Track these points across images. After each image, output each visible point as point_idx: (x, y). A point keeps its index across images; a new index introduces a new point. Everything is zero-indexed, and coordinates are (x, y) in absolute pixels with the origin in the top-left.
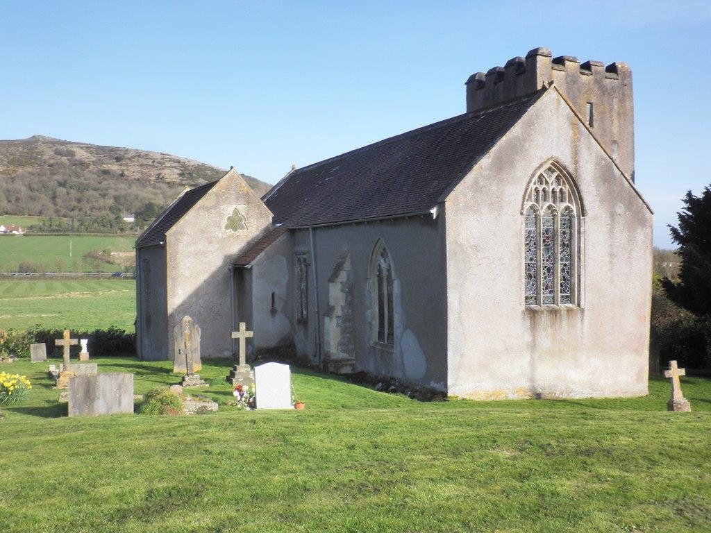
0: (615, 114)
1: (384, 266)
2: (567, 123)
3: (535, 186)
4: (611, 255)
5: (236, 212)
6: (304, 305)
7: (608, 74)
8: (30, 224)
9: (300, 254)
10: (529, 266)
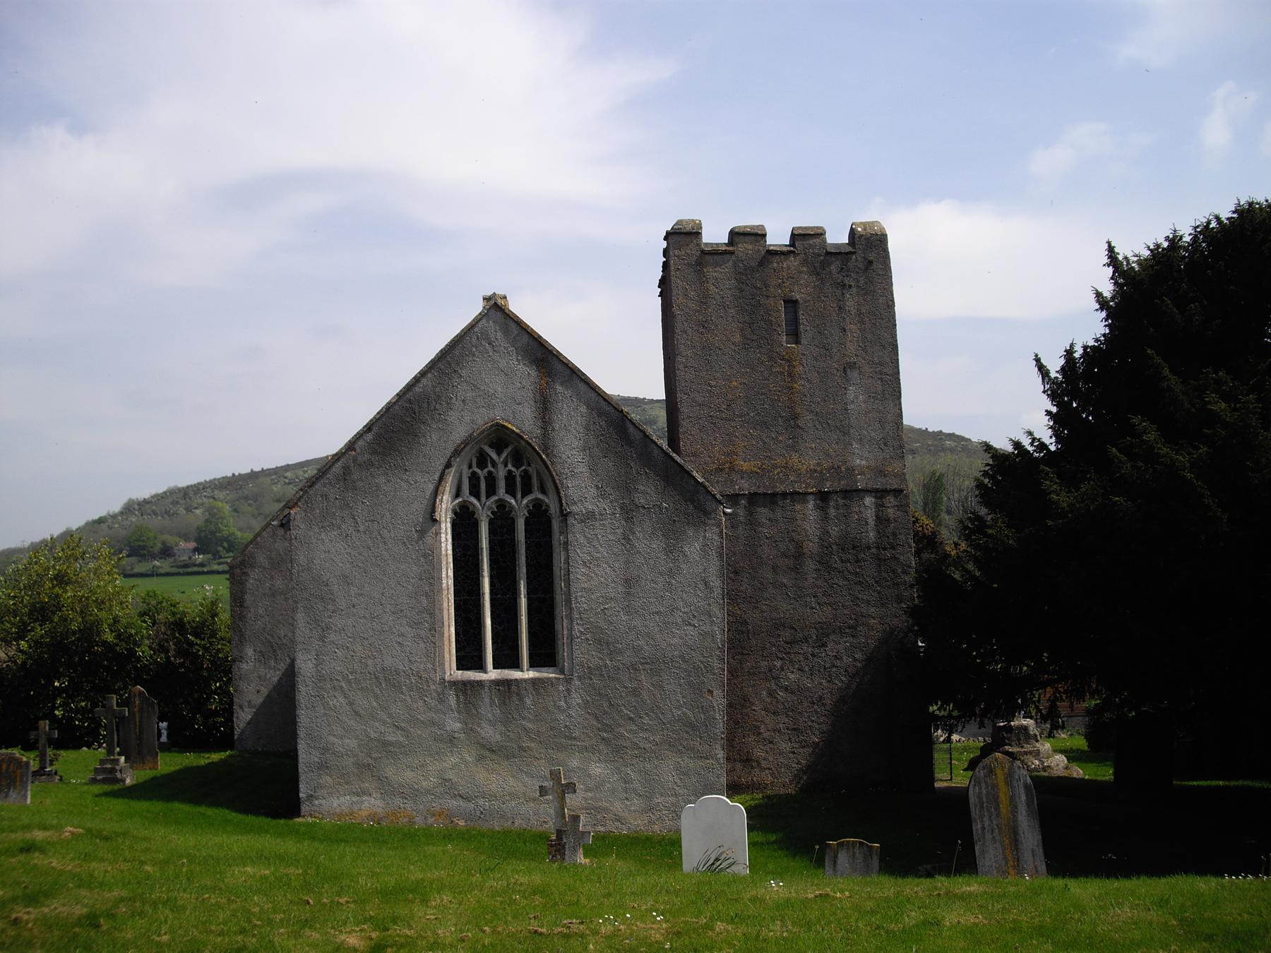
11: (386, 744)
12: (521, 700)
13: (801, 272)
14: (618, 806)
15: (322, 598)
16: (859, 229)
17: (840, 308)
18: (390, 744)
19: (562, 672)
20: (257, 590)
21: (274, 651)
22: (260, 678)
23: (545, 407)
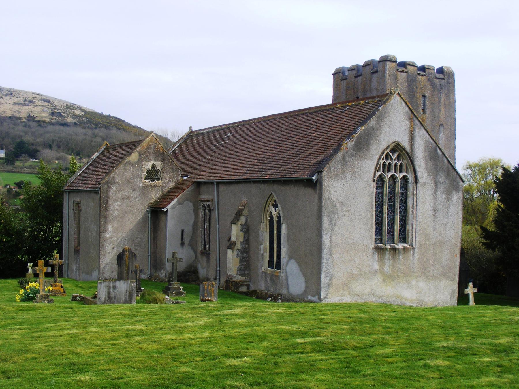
0: (442, 105)
1: (274, 213)
2: (406, 118)
3: (383, 161)
4: (434, 210)
5: (153, 166)
6: (207, 240)
7: (438, 75)
8: (17, 181)
9: (205, 201)
10: (378, 216)
16: (446, 70)
17: (439, 101)
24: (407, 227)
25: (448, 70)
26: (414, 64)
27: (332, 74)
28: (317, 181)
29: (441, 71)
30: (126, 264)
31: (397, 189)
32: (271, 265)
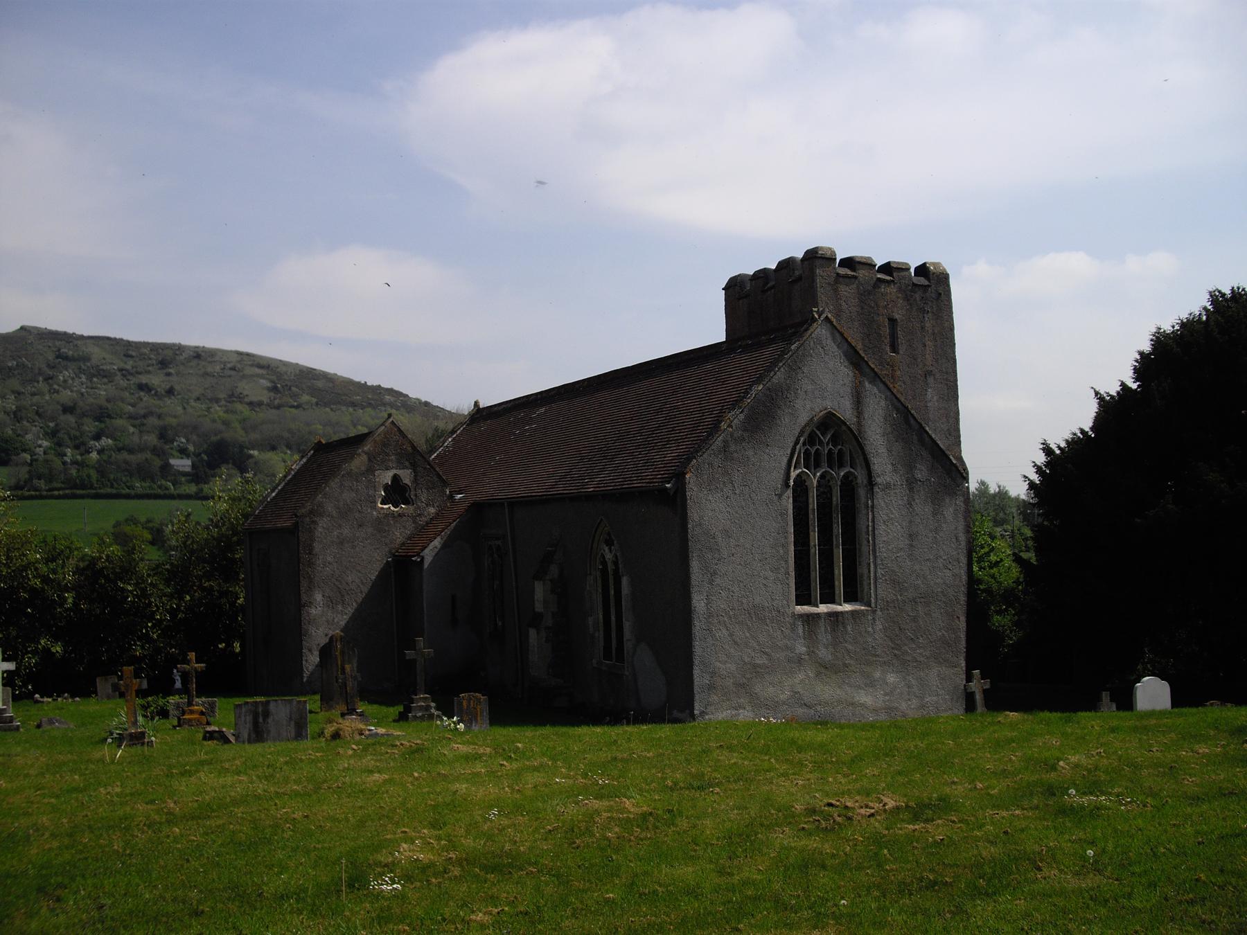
1: (609, 556)
5: (396, 478)
11: (755, 666)
12: (844, 627)
13: (898, 298)
14: (904, 706)
15: (711, 549)
16: (932, 268)
17: (922, 328)
18: (759, 666)
19: (869, 605)
20: (326, 538)
21: (343, 596)
22: (328, 621)
23: (858, 401)
24: (859, 571)
25: (935, 268)
26: (869, 262)
27: (723, 289)
28: (675, 493)
29: (922, 270)
30: (337, 664)
31: (834, 499)
32: (607, 655)
